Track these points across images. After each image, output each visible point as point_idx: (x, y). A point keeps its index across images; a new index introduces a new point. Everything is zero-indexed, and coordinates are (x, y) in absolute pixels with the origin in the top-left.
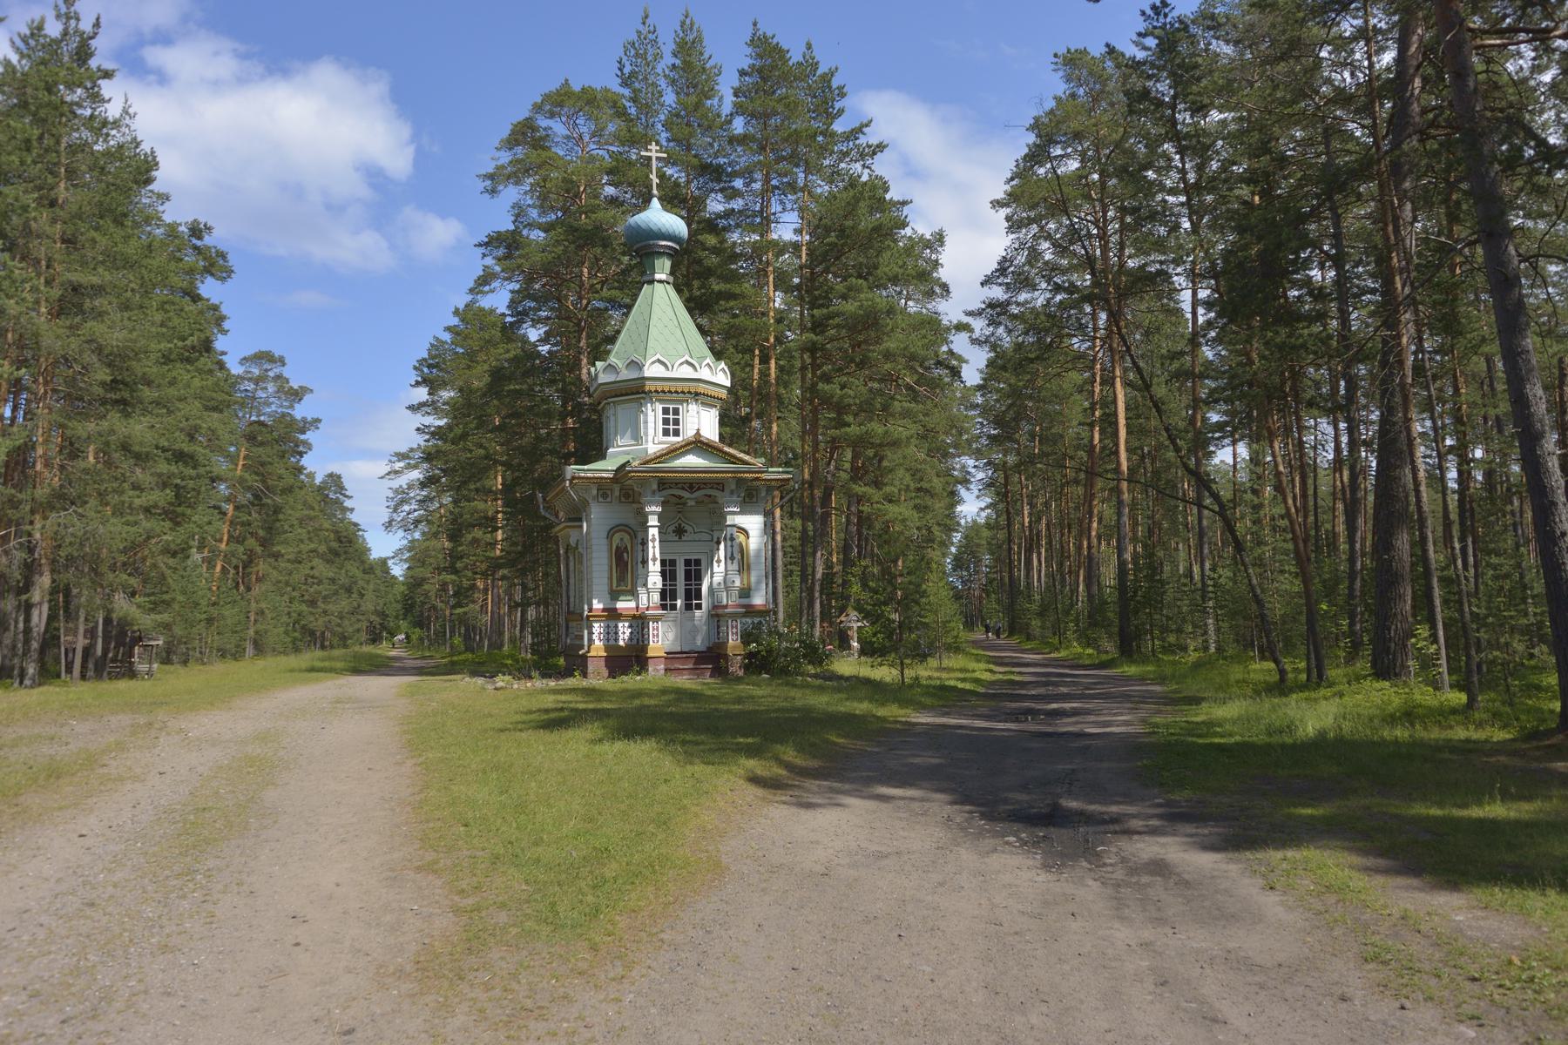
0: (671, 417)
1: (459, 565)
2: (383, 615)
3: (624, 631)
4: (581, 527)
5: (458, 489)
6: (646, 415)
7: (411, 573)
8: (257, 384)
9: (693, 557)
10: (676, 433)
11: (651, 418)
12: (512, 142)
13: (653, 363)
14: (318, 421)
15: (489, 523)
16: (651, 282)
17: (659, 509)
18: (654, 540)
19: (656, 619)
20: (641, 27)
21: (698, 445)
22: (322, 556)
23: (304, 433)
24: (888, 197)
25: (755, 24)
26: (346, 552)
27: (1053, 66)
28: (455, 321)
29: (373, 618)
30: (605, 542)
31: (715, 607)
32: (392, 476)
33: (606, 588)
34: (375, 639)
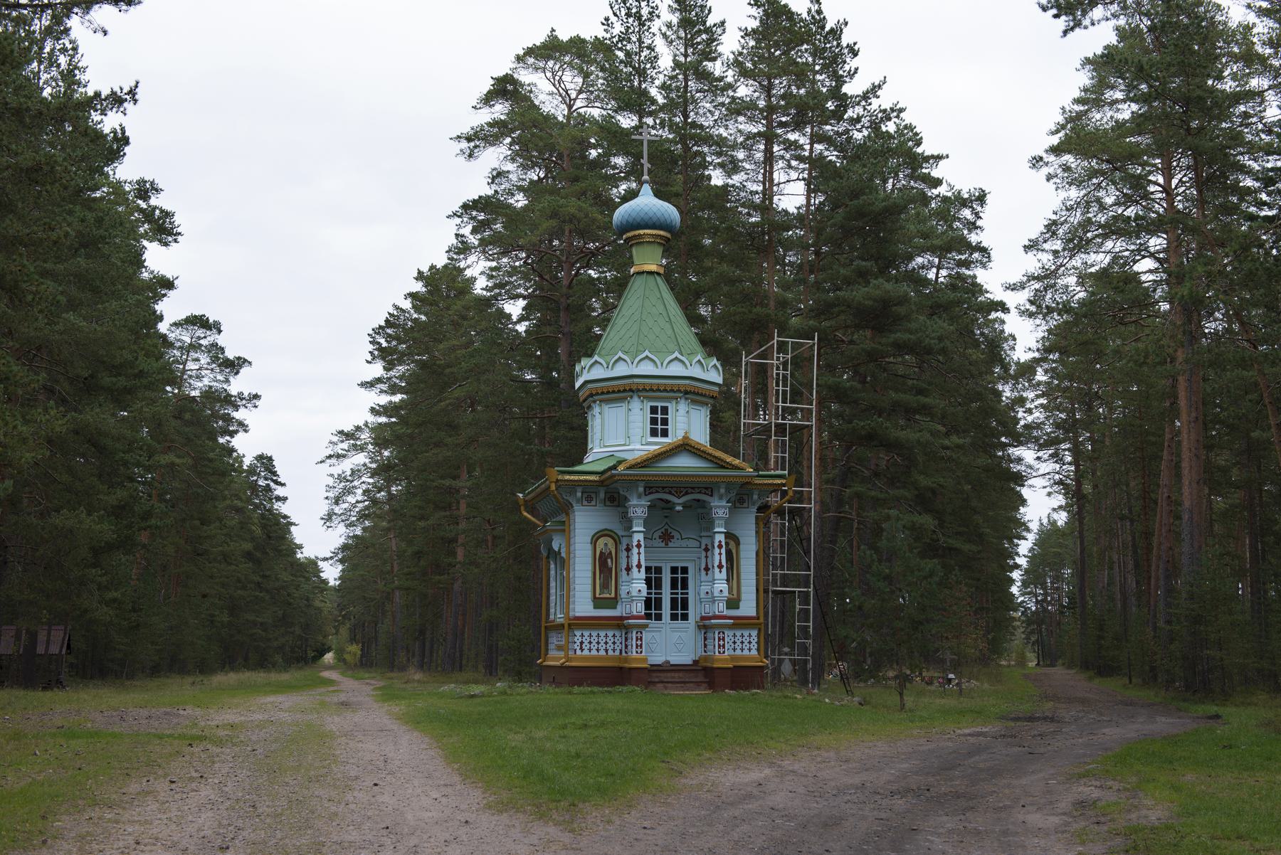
0: (659, 416)
9: (680, 565)
10: (665, 433)
21: (686, 447)
23: (236, 408)
24: (919, 150)
28: (418, 287)
30: (589, 547)
32: (333, 461)
33: (589, 595)
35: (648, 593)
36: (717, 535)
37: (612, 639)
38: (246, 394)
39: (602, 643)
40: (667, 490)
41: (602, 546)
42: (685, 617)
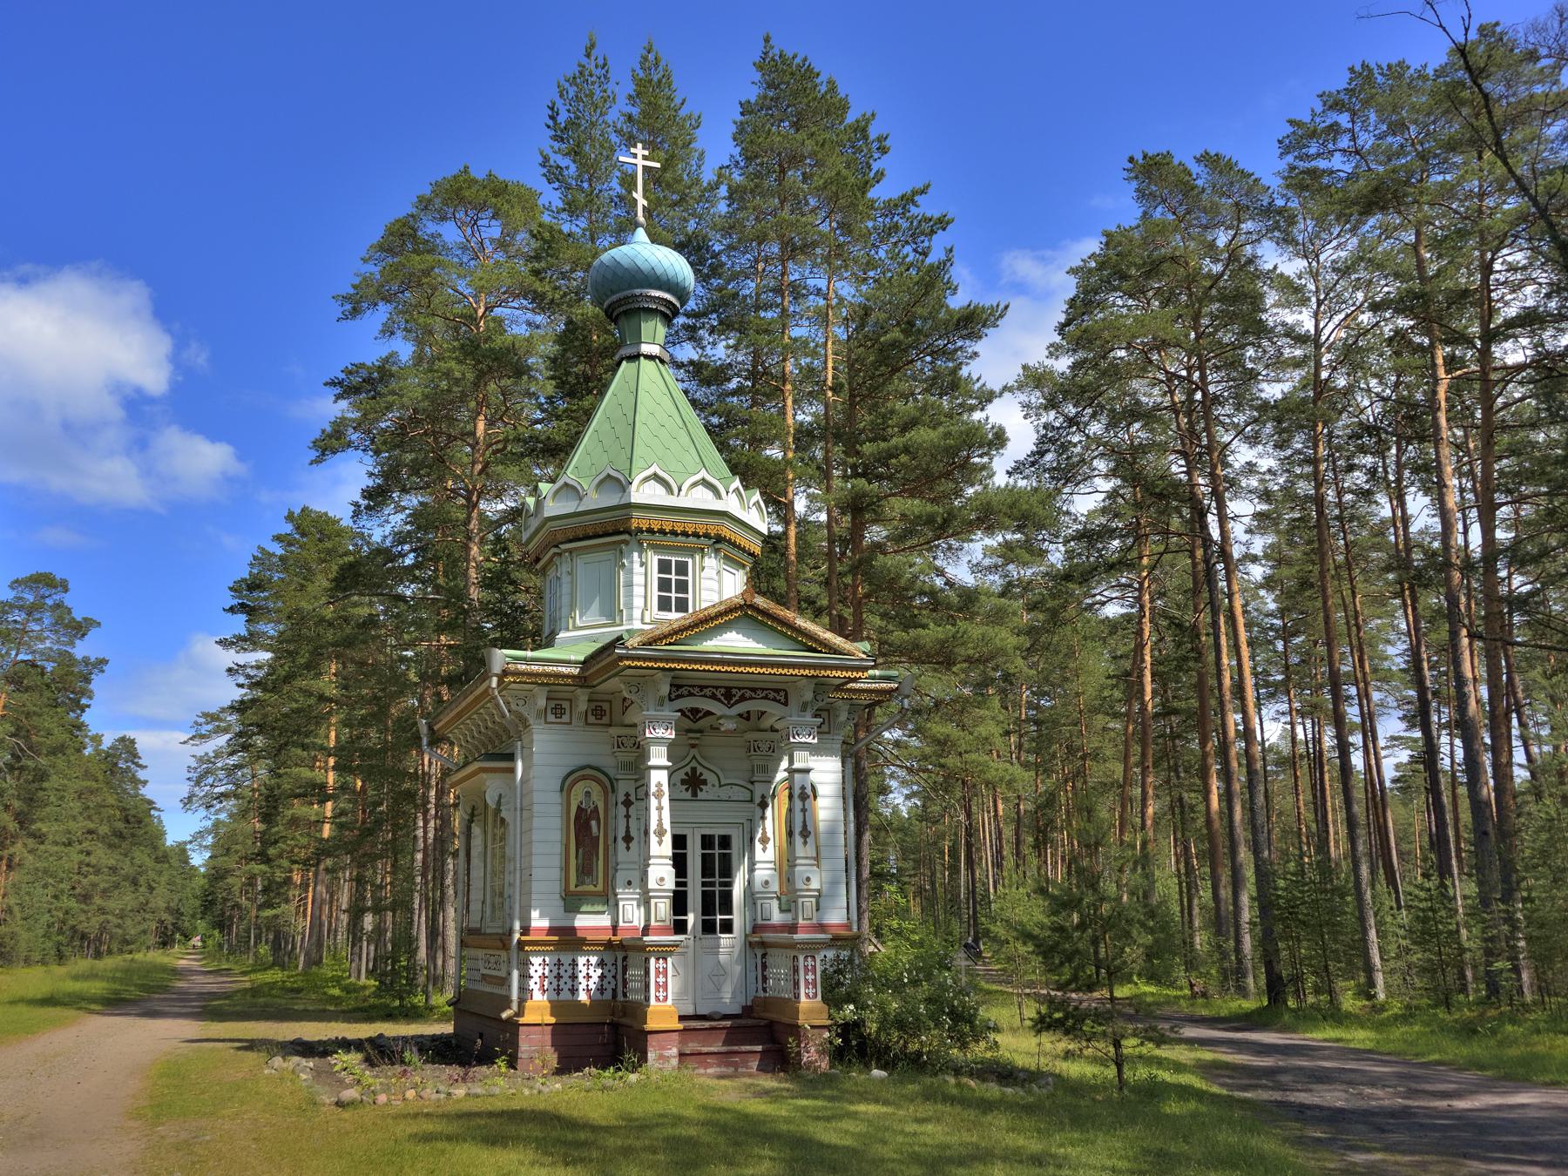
0: (673, 577)
1: (272, 851)
2: (178, 913)
3: (589, 973)
4: (512, 771)
5: (276, 753)
6: (631, 572)
7: (213, 863)
8: (29, 614)
9: (717, 832)
10: (682, 606)
11: (638, 579)
12: (385, 248)
13: (646, 479)
14: (104, 662)
15: (318, 792)
16: (635, 357)
17: (671, 735)
19: (663, 952)
20: (584, 61)
22: (103, 839)
25: (767, 40)
26: (133, 835)
27: (1125, 174)
28: (288, 528)
29: (165, 916)
30: (557, 797)
31: (756, 929)
32: (197, 742)
33: (556, 887)
34: (165, 942)
35: (678, 884)
36: (653, 773)
38: (93, 660)
40: (707, 691)
41: (581, 797)
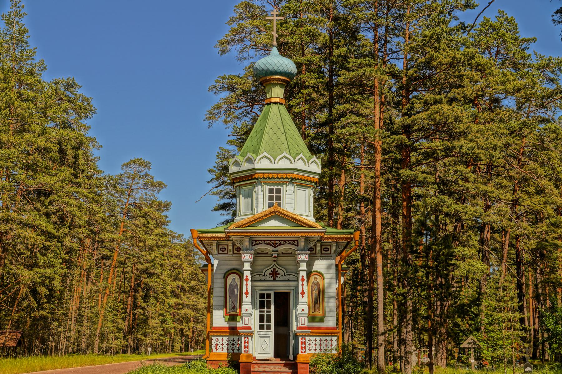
0: (275, 195)
6: (258, 195)
9: (265, 292)
11: (261, 197)
13: (281, 158)
16: (269, 104)
18: (247, 280)
30: (223, 281)
36: (300, 272)
37: (314, 342)
39: (313, 345)
40: (267, 242)
41: (231, 280)
42: (268, 328)
